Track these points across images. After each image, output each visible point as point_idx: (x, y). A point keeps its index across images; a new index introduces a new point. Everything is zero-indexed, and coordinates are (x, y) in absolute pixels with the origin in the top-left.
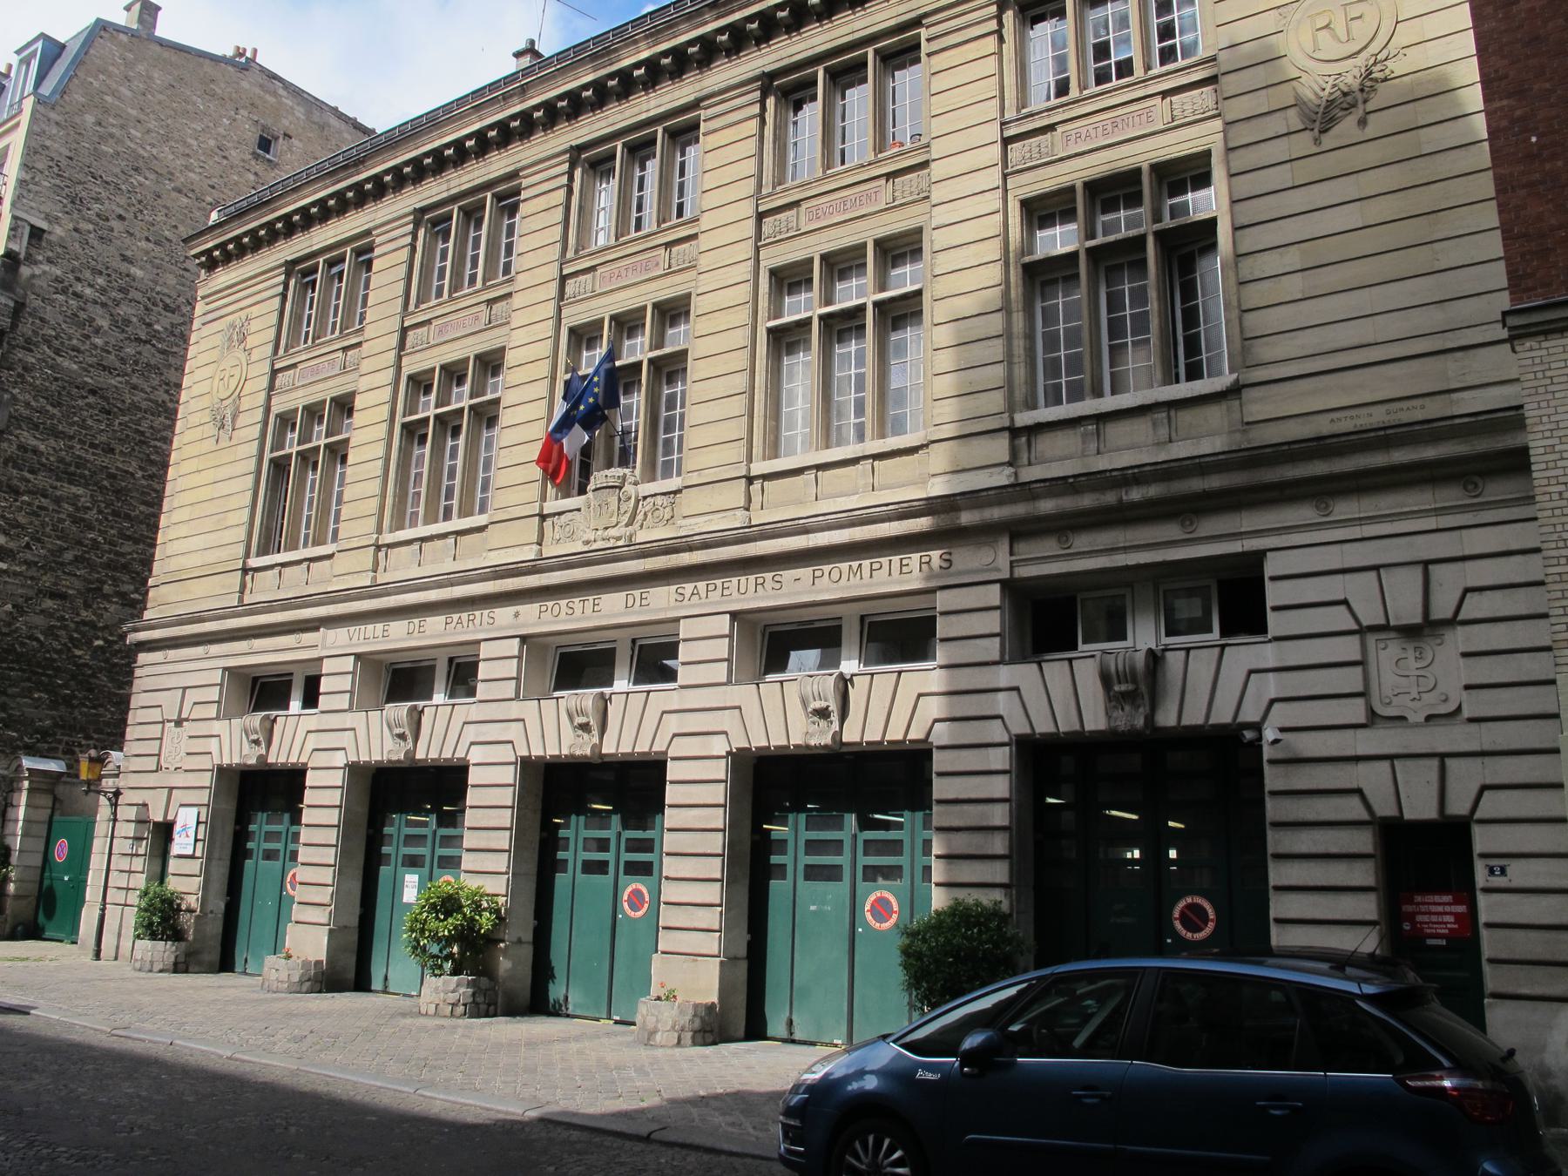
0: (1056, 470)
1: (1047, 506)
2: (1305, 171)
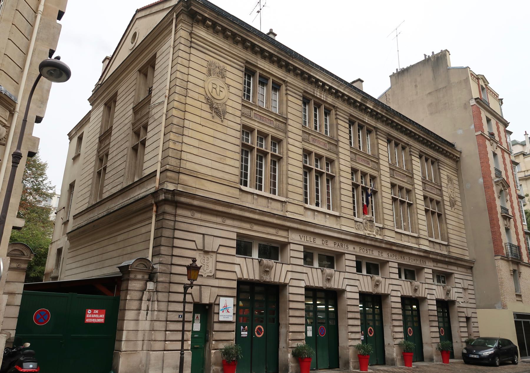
2: (203, 122)
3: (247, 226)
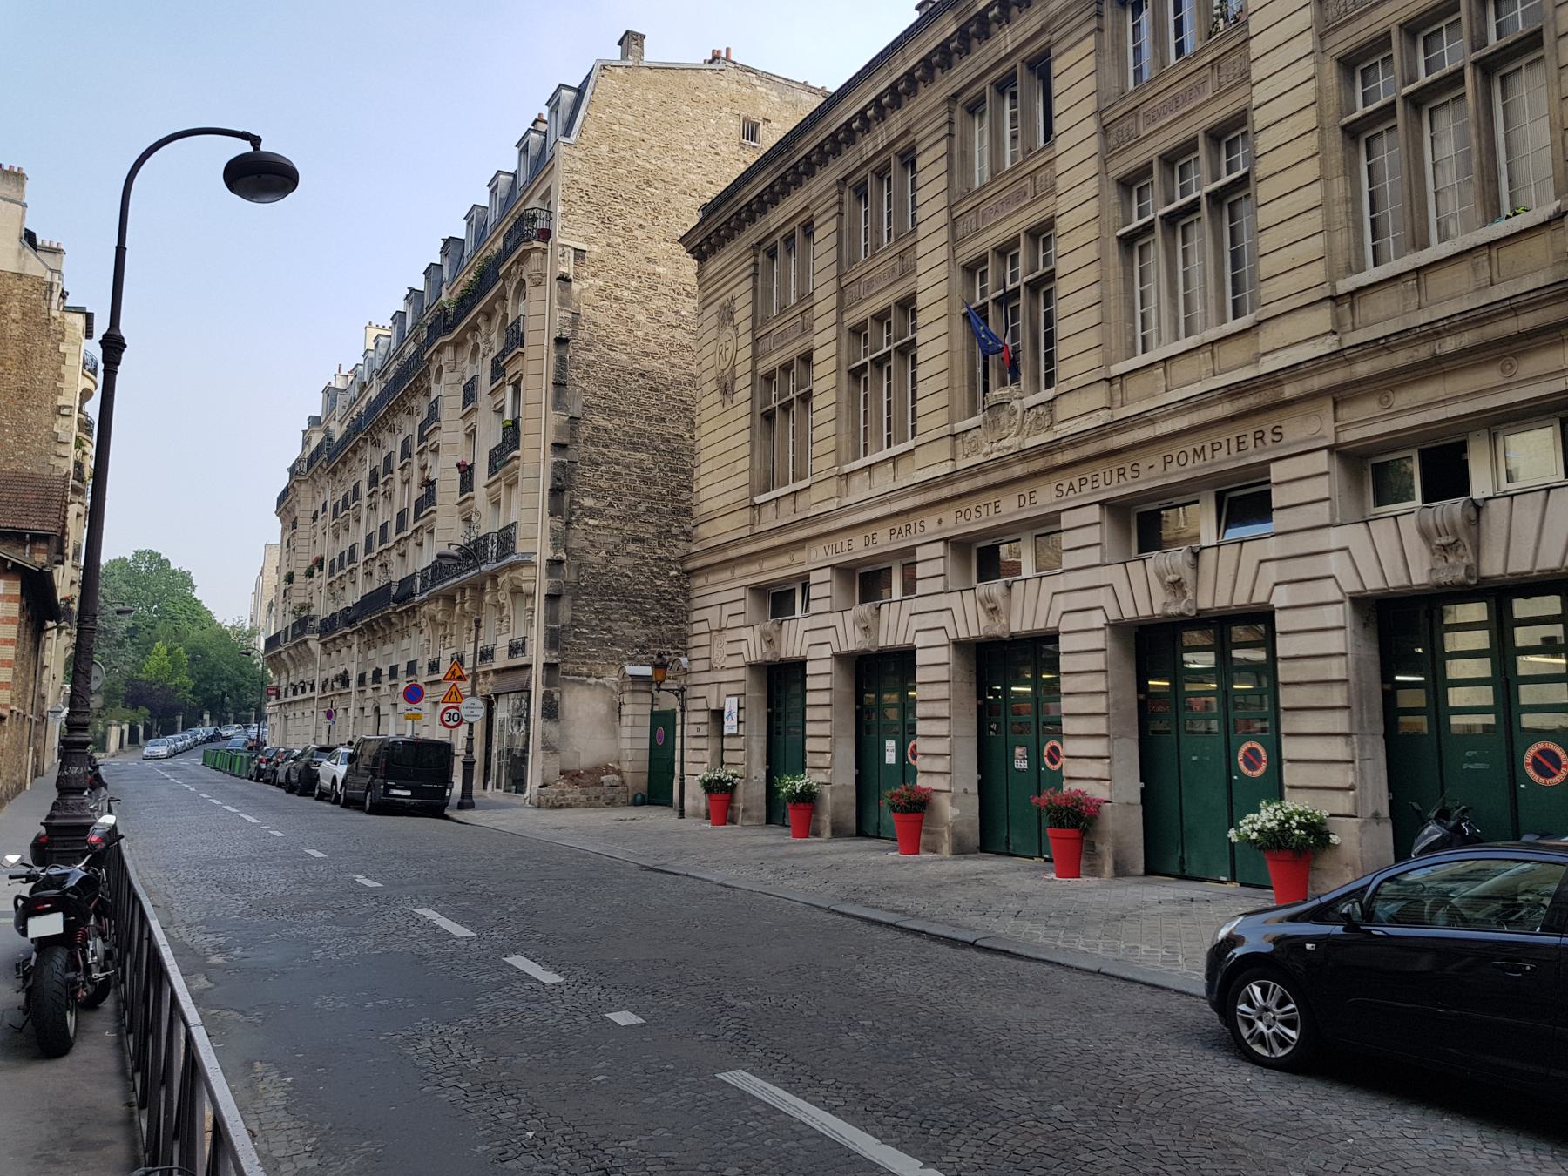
0: (1378, 331)
1: (1363, 369)
3: (755, 568)
